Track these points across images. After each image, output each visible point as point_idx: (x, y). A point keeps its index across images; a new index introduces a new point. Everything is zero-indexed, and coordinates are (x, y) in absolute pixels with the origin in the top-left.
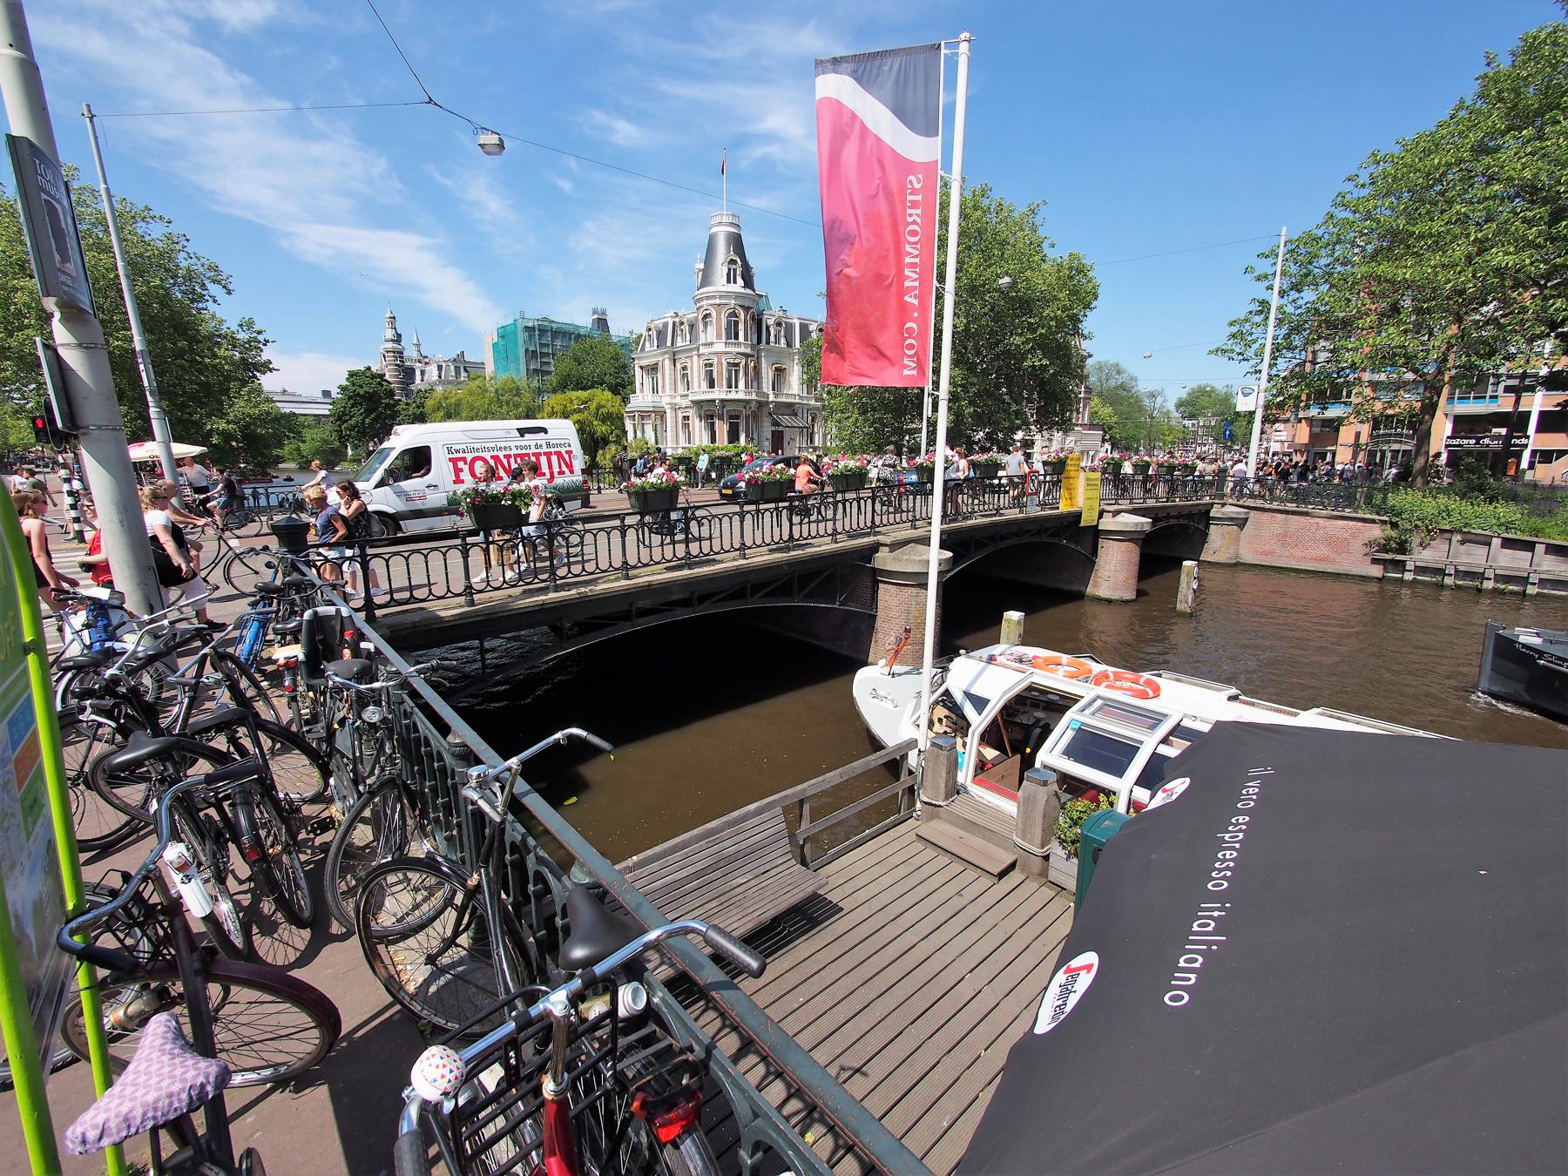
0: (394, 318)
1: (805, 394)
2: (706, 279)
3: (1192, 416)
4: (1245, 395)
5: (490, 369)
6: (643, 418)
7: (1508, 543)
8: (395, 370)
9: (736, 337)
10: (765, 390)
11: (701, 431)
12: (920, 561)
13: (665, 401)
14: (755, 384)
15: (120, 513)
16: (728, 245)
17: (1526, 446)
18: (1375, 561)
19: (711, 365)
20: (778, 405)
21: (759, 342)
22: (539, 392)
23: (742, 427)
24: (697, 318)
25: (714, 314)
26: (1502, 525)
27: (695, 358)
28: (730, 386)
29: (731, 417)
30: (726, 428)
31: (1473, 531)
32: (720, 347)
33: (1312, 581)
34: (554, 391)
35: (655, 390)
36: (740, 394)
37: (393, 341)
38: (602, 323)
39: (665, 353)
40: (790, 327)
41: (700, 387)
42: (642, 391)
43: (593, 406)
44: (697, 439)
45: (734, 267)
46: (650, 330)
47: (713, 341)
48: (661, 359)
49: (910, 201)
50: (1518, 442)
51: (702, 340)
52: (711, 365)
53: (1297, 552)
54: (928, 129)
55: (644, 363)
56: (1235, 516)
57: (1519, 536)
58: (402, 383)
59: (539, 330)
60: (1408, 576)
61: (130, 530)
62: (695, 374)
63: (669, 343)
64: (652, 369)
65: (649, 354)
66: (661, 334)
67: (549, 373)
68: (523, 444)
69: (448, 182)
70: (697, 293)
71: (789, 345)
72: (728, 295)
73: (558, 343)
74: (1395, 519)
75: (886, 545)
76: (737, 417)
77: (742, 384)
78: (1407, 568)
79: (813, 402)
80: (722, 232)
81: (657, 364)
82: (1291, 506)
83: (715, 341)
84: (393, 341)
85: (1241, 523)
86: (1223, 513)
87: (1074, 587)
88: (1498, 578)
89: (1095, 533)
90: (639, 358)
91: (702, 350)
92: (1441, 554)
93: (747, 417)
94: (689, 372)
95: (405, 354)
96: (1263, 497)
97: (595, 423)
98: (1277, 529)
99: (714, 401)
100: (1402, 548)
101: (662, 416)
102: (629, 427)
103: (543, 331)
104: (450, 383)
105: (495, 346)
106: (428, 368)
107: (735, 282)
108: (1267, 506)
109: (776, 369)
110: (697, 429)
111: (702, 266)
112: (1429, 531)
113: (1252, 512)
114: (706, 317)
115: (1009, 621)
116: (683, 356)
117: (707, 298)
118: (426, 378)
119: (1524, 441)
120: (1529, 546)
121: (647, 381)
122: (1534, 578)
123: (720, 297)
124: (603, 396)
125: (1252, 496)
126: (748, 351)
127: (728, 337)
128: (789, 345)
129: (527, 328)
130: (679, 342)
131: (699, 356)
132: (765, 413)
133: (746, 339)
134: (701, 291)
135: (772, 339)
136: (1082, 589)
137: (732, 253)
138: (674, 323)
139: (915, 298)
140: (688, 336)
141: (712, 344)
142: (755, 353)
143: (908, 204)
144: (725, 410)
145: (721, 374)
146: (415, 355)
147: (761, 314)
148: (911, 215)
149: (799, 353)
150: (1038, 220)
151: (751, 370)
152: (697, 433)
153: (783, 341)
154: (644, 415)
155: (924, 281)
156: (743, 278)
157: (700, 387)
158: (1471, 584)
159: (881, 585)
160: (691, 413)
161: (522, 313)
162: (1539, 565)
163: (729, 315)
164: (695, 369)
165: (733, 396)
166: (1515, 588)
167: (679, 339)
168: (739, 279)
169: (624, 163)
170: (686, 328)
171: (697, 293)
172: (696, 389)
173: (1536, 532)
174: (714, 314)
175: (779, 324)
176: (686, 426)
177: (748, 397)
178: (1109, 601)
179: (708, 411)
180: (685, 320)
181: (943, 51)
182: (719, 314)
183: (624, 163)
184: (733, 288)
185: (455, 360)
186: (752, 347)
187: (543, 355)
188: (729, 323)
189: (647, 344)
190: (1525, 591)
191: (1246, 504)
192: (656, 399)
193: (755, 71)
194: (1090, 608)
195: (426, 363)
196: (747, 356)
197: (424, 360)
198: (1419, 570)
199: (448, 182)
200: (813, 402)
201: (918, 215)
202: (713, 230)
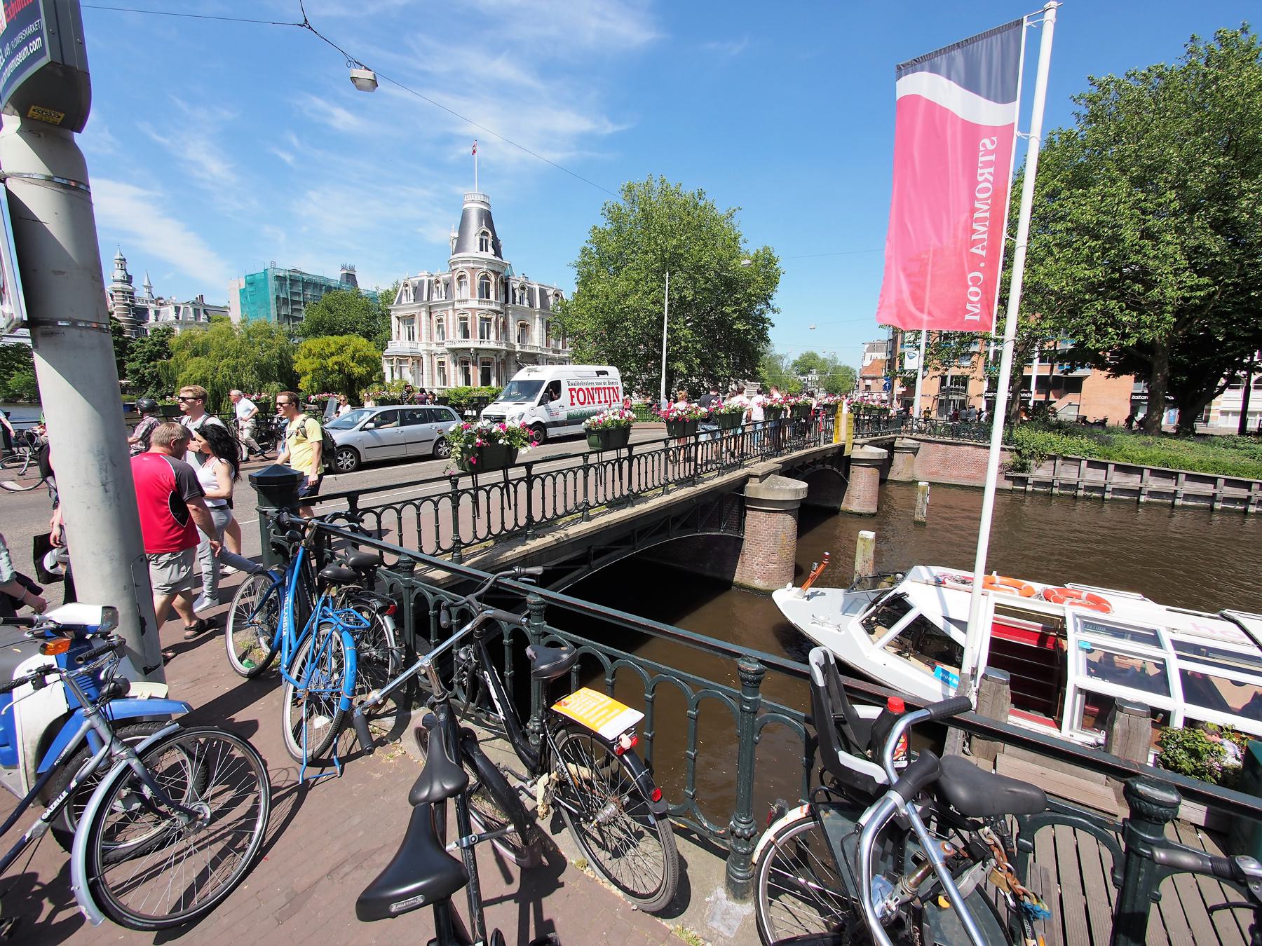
0: (124, 260)
1: (545, 347)
2: (460, 245)
3: (803, 374)
4: (910, 358)
5: (235, 316)
6: (400, 362)
7: (1091, 464)
8: (124, 309)
9: (488, 297)
10: (512, 342)
11: (456, 375)
12: (790, 490)
13: (421, 347)
14: (504, 336)
15: (103, 469)
16: (480, 219)
17: (1030, 398)
18: (1007, 478)
19: (466, 319)
20: (524, 354)
21: (507, 301)
22: (290, 336)
23: (493, 372)
24: (452, 278)
25: (468, 275)
26: (1086, 452)
27: (451, 312)
28: (482, 337)
29: (483, 363)
30: (479, 372)
31: (1069, 456)
32: (474, 304)
33: (962, 493)
34: (305, 336)
35: (411, 337)
36: (491, 343)
37: (122, 281)
38: (350, 278)
39: (422, 306)
40: (531, 291)
41: (455, 336)
42: (398, 338)
43: (350, 350)
44: (452, 381)
45: (486, 237)
46: (407, 285)
47: (468, 299)
48: (418, 311)
49: (981, 162)
50: (1026, 395)
51: (457, 297)
52: (466, 319)
53: (955, 473)
54: (1005, 96)
55: (400, 314)
56: (912, 446)
57: (1097, 459)
58: (131, 321)
59: (290, 280)
60: (1029, 488)
61: (118, 496)
62: (451, 326)
63: (425, 298)
64: (409, 320)
65: (406, 305)
66: (417, 290)
67: (301, 319)
68: (599, 381)
69: (165, 141)
70: (453, 257)
71: (531, 305)
72: (481, 261)
73: (309, 292)
74: (1019, 448)
75: (757, 476)
76: (489, 364)
77: (493, 336)
78: (1029, 482)
79: (551, 353)
80: (474, 209)
81: (414, 315)
82: (948, 439)
83: (469, 298)
84: (122, 281)
85: (915, 451)
86: (904, 444)
87: (831, 505)
88: (1087, 488)
89: (849, 461)
90: (395, 310)
91: (457, 306)
92: (1049, 472)
93: (498, 364)
94: (444, 323)
95: (136, 295)
96: (930, 433)
97: (352, 364)
98: (939, 456)
99: (469, 349)
100: (1023, 468)
101: (419, 361)
102: (386, 368)
103: (294, 281)
104: (188, 324)
105: (243, 292)
106: (163, 309)
107: (487, 250)
108: (933, 439)
109: (521, 325)
110: (452, 373)
111: (456, 235)
112: (1041, 456)
113: (922, 444)
114: (460, 277)
115: (864, 540)
116: (439, 310)
117: (462, 262)
118: (161, 318)
119: (1029, 395)
120: (1104, 466)
121: (404, 331)
122: (1081, 485)
123: (474, 262)
124: (359, 342)
125: (920, 431)
126: (498, 308)
127: (481, 296)
128: (531, 305)
129: (278, 277)
130: (435, 298)
131: (454, 310)
132: (512, 358)
133: (496, 298)
134: (456, 255)
135: (517, 300)
136: (837, 505)
137: (484, 226)
138: (429, 281)
139: (982, 249)
140: (443, 292)
141: (467, 301)
142: (503, 311)
143: (980, 165)
144: (479, 357)
145: (474, 325)
146: (146, 296)
147: (508, 278)
148: (982, 175)
149: (539, 313)
150: (735, 221)
151: (500, 325)
152: (452, 377)
153: (526, 302)
154: (402, 359)
155: (994, 233)
156: (494, 248)
157: (455, 336)
158: (1070, 493)
159: (748, 512)
160: (446, 359)
161: (273, 263)
162: (1111, 479)
163: (483, 278)
164: (451, 321)
165: (485, 345)
166: (1097, 495)
167: (435, 295)
168: (490, 248)
169: (345, 144)
170: (442, 286)
171: (453, 257)
172: (451, 338)
173: (1109, 456)
174: (468, 275)
175: (523, 288)
176: (442, 370)
177: (499, 347)
178: (860, 515)
179: (463, 358)
180: (441, 279)
181: (1025, 24)
182: (472, 276)
183: (345, 144)
184: (484, 255)
185: (194, 303)
186: (501, 305)
187: (294, 302)
188: (481, 285)
189: (404, 297)
190: (1103, 497)
191: (917, 437)
192: (414, 345)
193: (461, 85)
194: (840, 518)
195: (161, 304)
196: (497, 312)
197: (160, 302)
198: (1036, 484)
199: (165, 141)
200: (551, 353)
201: (990, 174)
202: (466, 206)
